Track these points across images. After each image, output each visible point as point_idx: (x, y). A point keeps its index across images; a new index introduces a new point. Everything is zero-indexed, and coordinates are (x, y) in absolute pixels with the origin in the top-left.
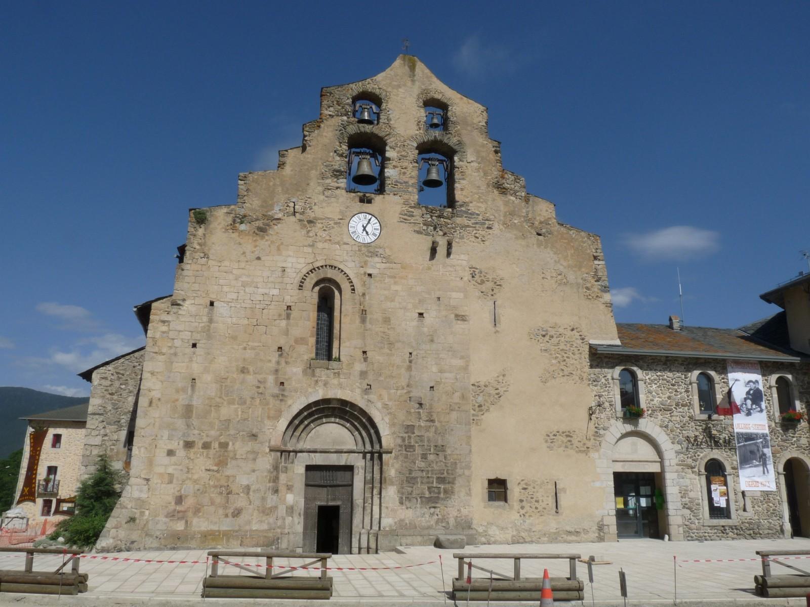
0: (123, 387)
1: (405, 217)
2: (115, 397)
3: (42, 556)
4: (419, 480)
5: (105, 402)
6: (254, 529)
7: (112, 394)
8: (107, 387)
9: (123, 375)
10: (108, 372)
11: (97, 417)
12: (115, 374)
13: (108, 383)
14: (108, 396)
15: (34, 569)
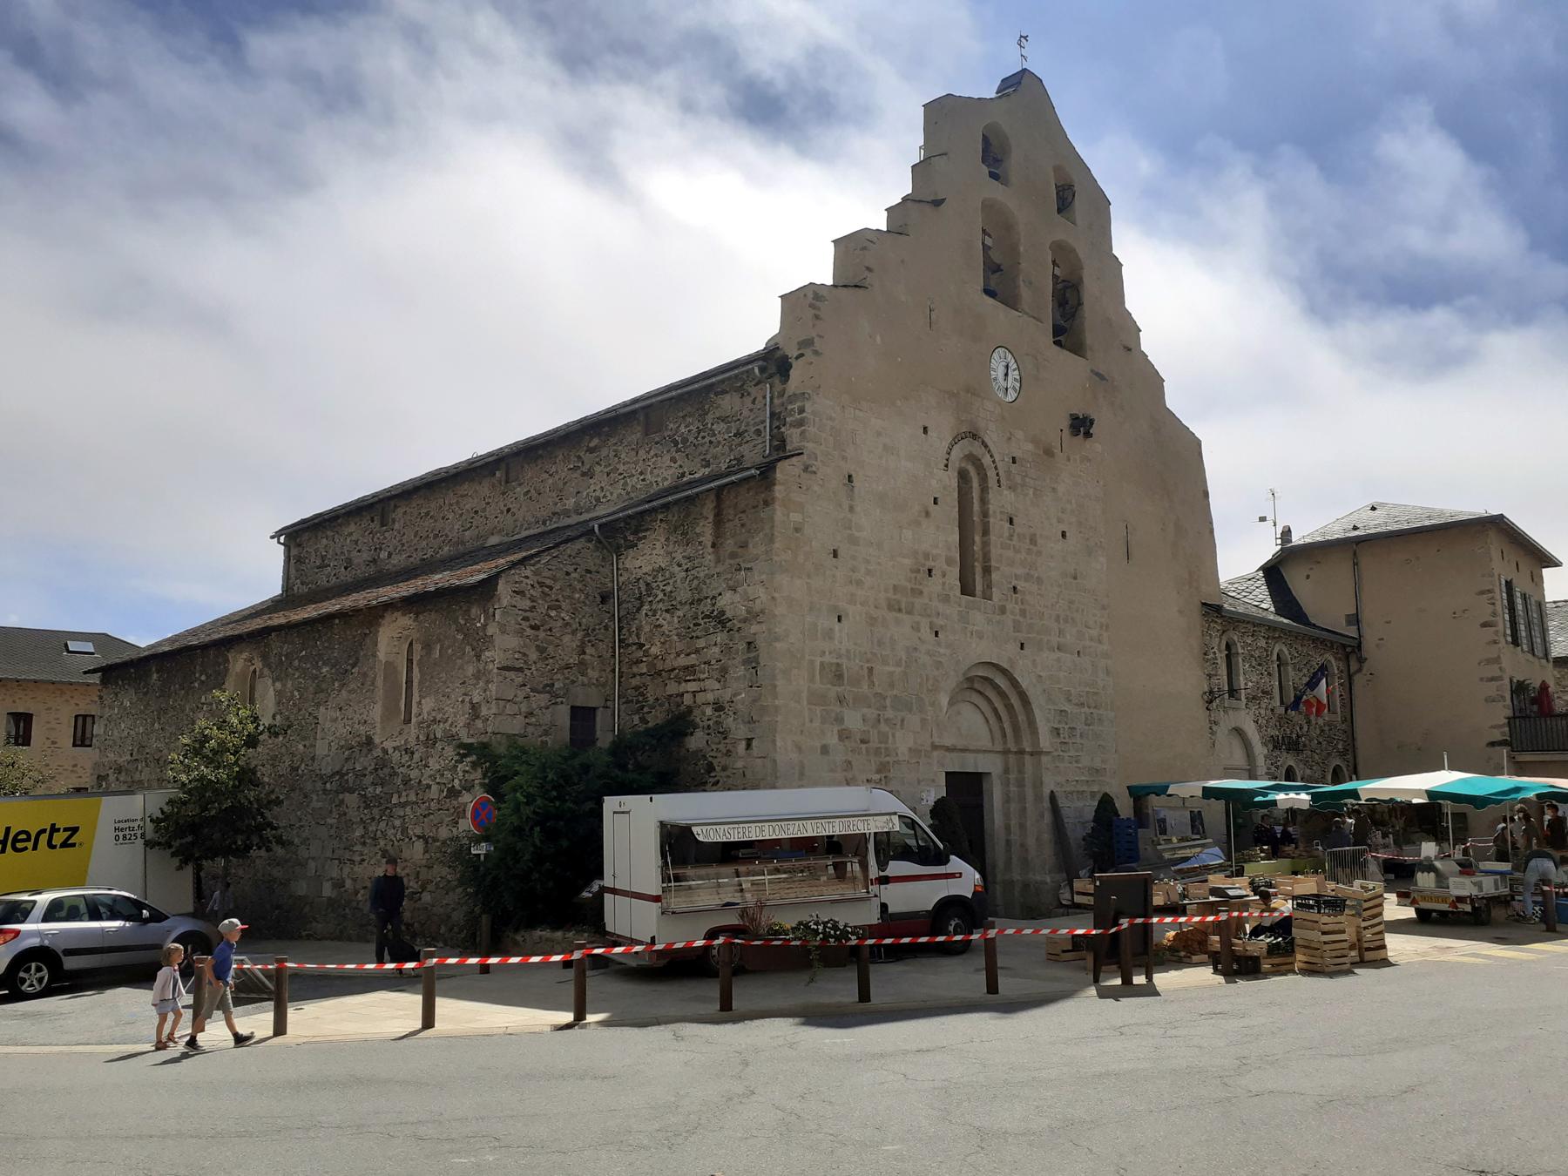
0: (553, 613)
1: (1555, 730)
2: (542, 635)
3: (894, 969)
4: (923, 753)
5: (525, 645)
6: (977, 876)
7: (535, 628)
8: (526, 611)
9: (551, 588)
10: (525, 580)
11: (512, 674)
12: (536, 585)
13: (527, 604)
14: (529, 632)
15: (418, 999)
